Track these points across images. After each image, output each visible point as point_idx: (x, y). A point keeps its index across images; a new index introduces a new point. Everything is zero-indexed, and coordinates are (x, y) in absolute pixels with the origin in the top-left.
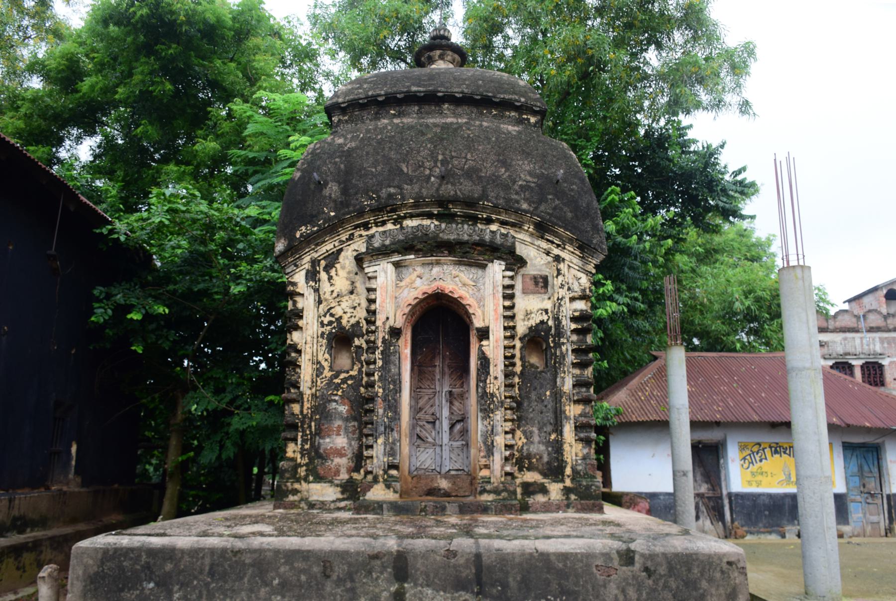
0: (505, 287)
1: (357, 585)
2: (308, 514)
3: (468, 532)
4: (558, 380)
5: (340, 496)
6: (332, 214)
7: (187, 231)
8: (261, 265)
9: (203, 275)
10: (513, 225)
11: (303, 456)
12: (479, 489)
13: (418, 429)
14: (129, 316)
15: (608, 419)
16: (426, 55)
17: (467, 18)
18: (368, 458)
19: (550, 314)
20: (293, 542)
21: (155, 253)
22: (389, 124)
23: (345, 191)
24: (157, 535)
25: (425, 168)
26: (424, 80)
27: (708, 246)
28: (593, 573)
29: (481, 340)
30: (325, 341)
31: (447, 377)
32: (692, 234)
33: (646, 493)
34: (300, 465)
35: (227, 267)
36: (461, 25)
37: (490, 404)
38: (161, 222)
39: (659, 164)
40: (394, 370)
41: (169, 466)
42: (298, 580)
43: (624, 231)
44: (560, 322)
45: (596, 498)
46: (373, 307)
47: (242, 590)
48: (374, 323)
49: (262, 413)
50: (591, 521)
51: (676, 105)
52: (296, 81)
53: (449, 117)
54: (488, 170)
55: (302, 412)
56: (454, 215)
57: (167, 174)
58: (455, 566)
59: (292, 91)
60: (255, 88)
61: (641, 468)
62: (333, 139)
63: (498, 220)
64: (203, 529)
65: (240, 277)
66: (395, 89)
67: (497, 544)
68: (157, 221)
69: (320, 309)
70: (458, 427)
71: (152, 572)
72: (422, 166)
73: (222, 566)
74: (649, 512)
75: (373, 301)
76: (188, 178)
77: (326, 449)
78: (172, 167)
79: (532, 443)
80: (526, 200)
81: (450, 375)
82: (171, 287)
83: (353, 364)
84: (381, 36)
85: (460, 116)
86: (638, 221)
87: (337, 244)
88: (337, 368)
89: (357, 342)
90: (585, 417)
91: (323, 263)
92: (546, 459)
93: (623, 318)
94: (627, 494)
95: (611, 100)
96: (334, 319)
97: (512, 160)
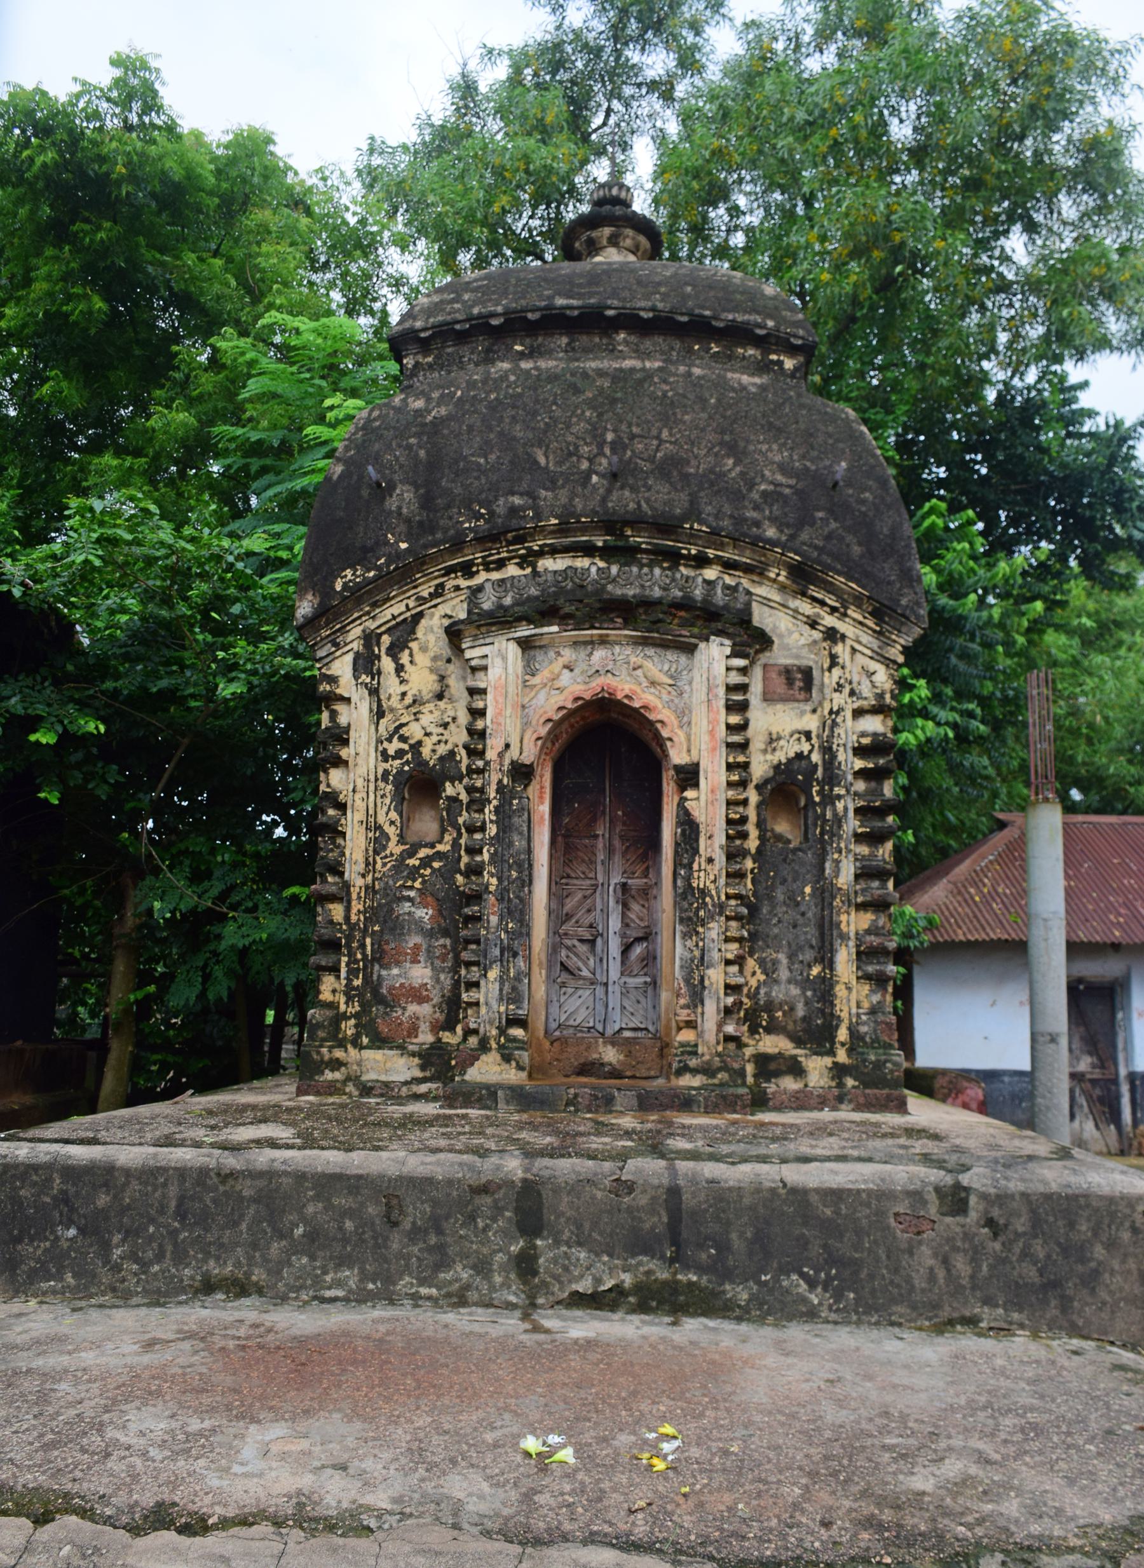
0: (730, 689)
2: (359, 1106)
3: (656, 1149)
4: (828, 865)
5: (419, 1074)
6: (404, 546)
7: (137, 580)
8: (273, 645)
9: (167, 663)
10: (748, 569)
11: (349, 999)
12: (675, 1065)
13: (564, 953)
14: (33, 738)
15: (912, 937)
16: (584, 238)
17: (660, 173)
18: (470, 1004)
19: (814, 741)
20: (330, 1159)
21: (78, 621)
22: (513, 371)
23: (426, 502)
24: (82, 1142)
25: (580, 457)
26: (580, 286)
27: (1104, 616)
28: (888, 1227)
29: (683, 789)
31: (617, 858)
32: (1077, 590)
33: (978, 1072)
34: (345, 1017)
35: (211, 648)
36: (649, 185)
38: (86, 562)
39: (1021, 458)
40: (518, 843)
41: (113, 1010)
42: (340, 1229)
43: (953, 586)
44: (833, 756)
45: (894, 1084)
46: (480, 724)
47: (237, 1244)
48: (481, 754)
49: (279, 917)
50: (885, 1129)
51: (1067, 339)
52: (336, 296)
53: (628, 358)
54: (700, 463)
55: (347, 918)
56: (636, 549)
57: (101, 473)
58: (630, 1210)
59: (329, 313)
60: (261, 308)
61: (973, 1027)
62: (404, 400)
63: (719, 560)
64: (166, 1131)
65: (235, 667)
66: (523, 302)
67: (710, 1169)
68: (79, 559)
69: (382, 728)
70: (638, 950)
71: (72, 1210)
72: (576, 453)
73: (201, 1200)
74: (983, 1108)
75: (480, 713)
76: (137, 480)
78: (108, 460)
79: (776, 981)
80: (773, 520)
81: (624, 854)
82: (109, 685)
83: (443, 831)
84: (496, 208)
85: (648, 355)
86: (978, 566)
87: (412, 604)
88: (412, 838)
89: (449, 790)
90: (877, 935)
91: (386, 640)
92: (800, 1011)
93: (944, 751)
94: (944, 1072)
95: (936, 333)
96: (406, 747)
97: (748, 441)
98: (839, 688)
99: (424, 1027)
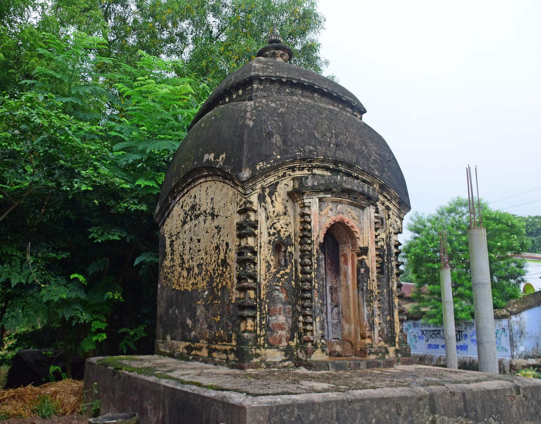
1: (414, 418)
4: (390, 283)
5: (284, 358)
6: (279, 157)
12: (368, 352)
23: (285, 142)
30: (271, 246)
34: (260, 336)
37: (370, 297)
42: (385, 418)
56: (340, 171)
73: (344, 413)
77: (273, 324)
96: (276, 232)
99: (284, 340)
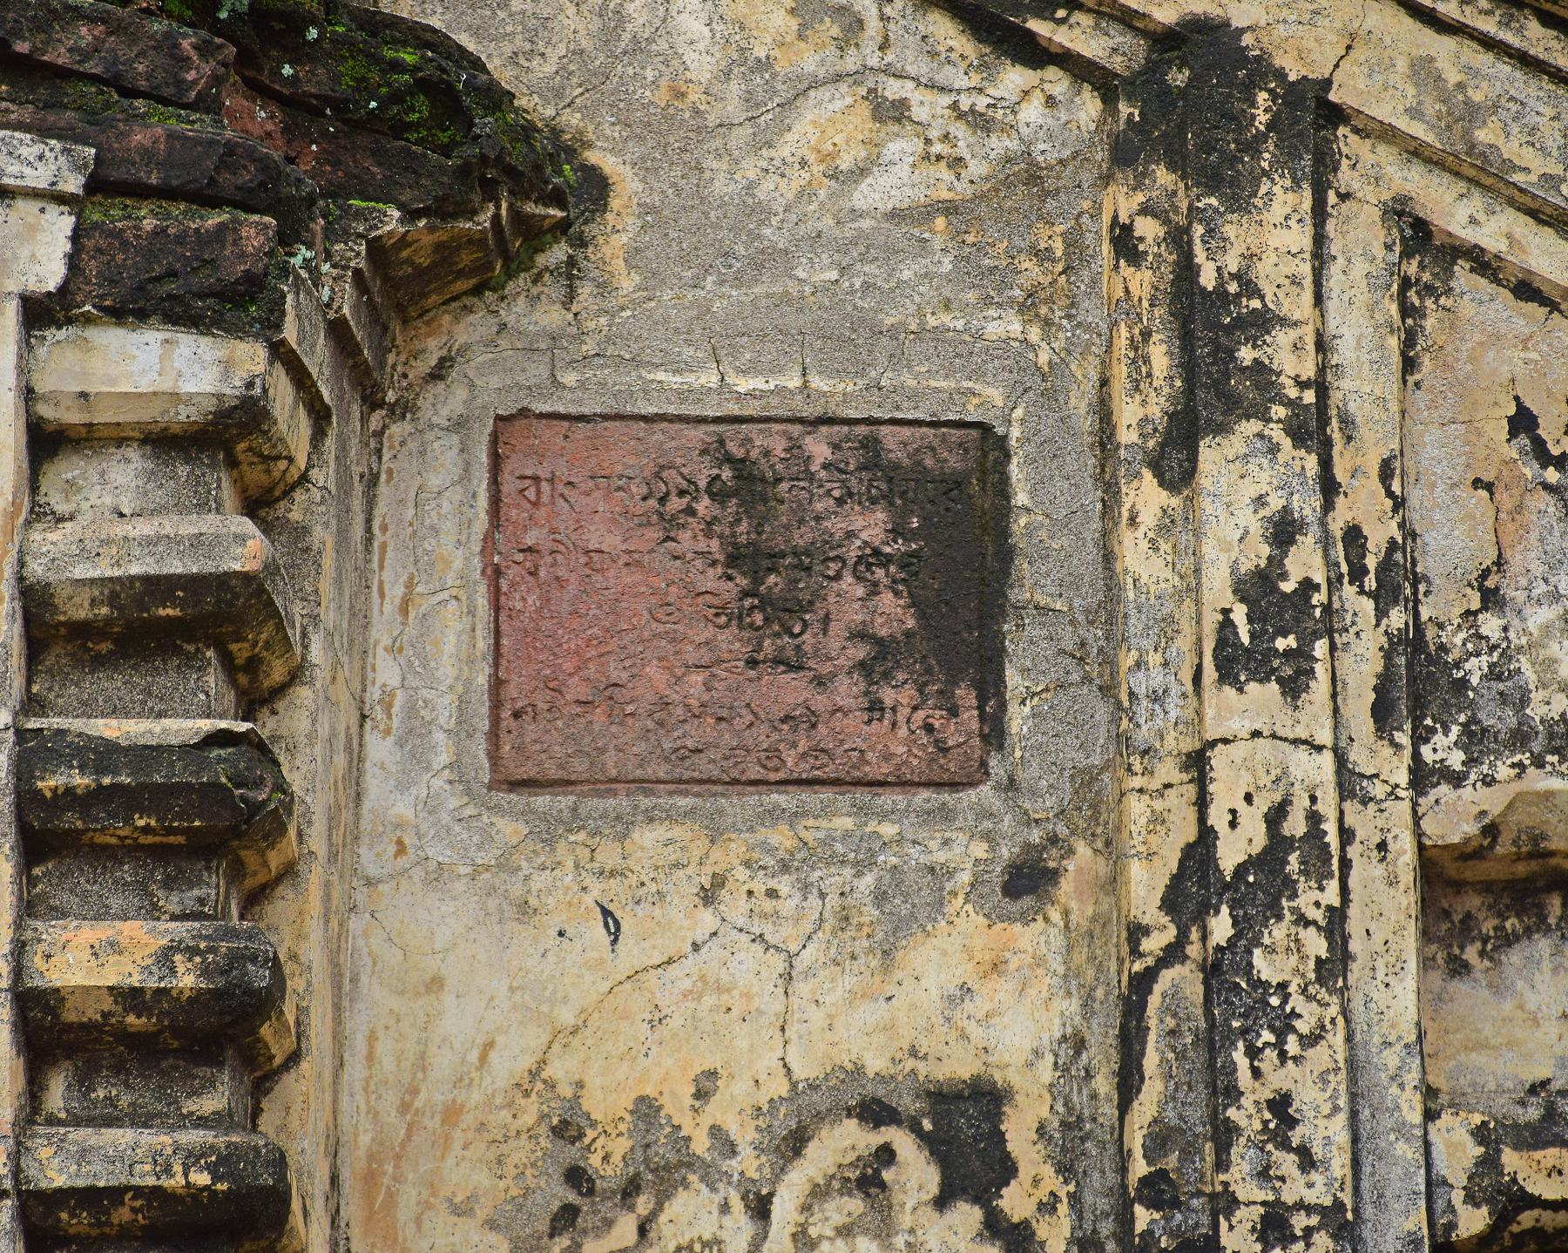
98: (1271, 634)
